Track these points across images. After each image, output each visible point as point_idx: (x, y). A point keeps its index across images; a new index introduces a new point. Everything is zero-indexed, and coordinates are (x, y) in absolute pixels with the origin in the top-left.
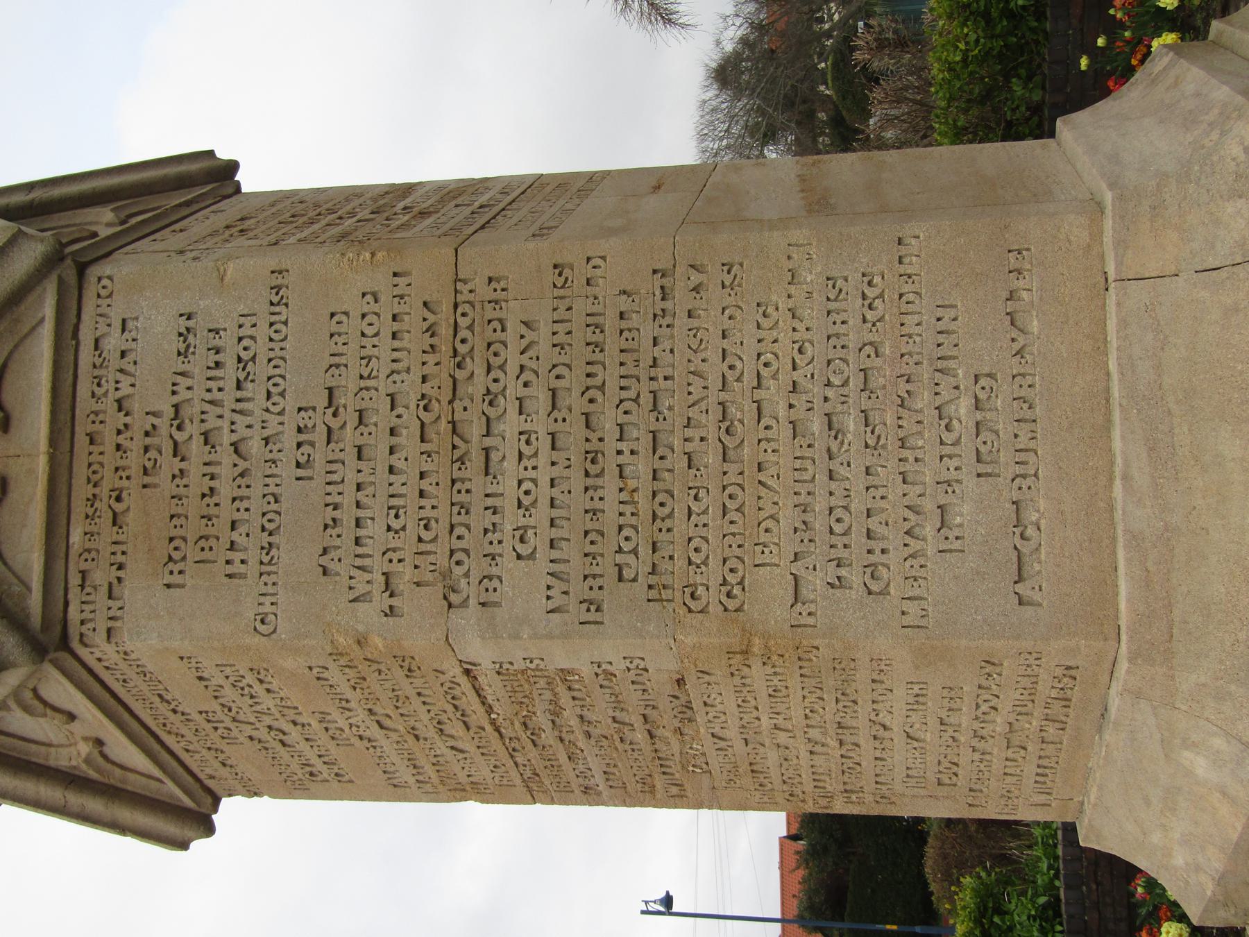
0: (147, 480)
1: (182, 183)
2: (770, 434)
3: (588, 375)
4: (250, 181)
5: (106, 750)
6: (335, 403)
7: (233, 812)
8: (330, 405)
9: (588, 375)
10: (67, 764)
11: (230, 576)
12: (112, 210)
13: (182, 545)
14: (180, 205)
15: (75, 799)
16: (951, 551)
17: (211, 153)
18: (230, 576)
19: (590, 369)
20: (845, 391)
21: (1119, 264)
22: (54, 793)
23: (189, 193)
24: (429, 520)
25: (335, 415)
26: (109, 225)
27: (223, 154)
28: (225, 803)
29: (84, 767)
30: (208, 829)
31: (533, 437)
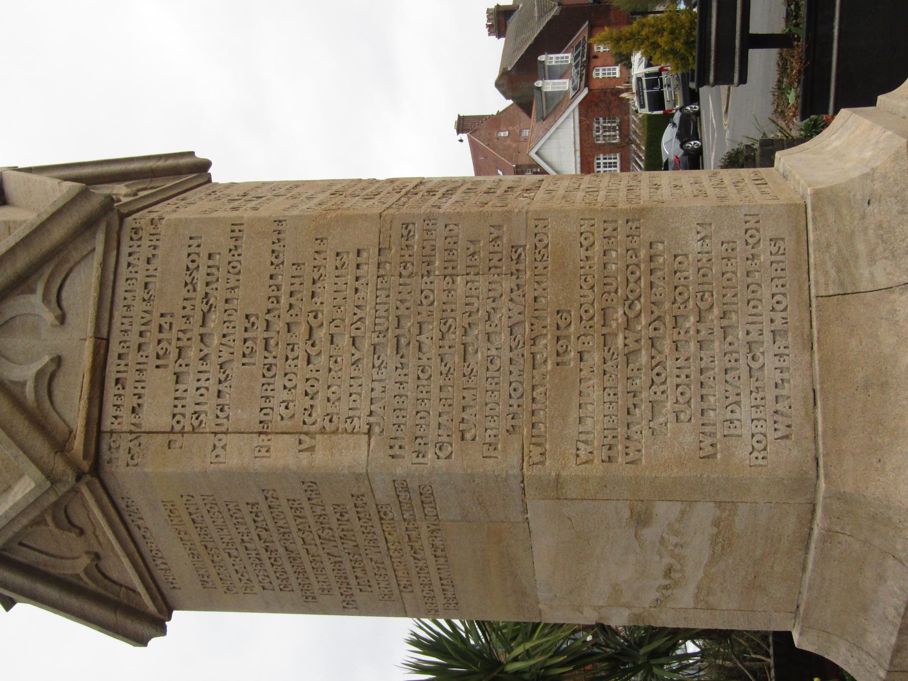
0: (159, 362)
1: (176, 171)
2: (231, 318)
3: (208, 274)
4: (218, 175)
5: (104, 564)
6: (314, 338)
7: (179, 620)
8: (310, 339)
9: (208, 274)
10: (70, 572)
11: (393, 457)
12: (126, 186)
13: (182, 420)
14: (170, 188)
15: (74, 602)
16: (490, 457)
17: (192, 154)
18: (393, 457)
19: (209, 271)
20: (431, 308)
21: (817, 291)
22: (53, 593)
23: (179, 179)
24: (223, 405)
25: (313, 345)
26: (125, 196)
27: (200, 155)
28: (176, 614)
29: (86, 579)
30: (162, 631)
31: (296, 346)
